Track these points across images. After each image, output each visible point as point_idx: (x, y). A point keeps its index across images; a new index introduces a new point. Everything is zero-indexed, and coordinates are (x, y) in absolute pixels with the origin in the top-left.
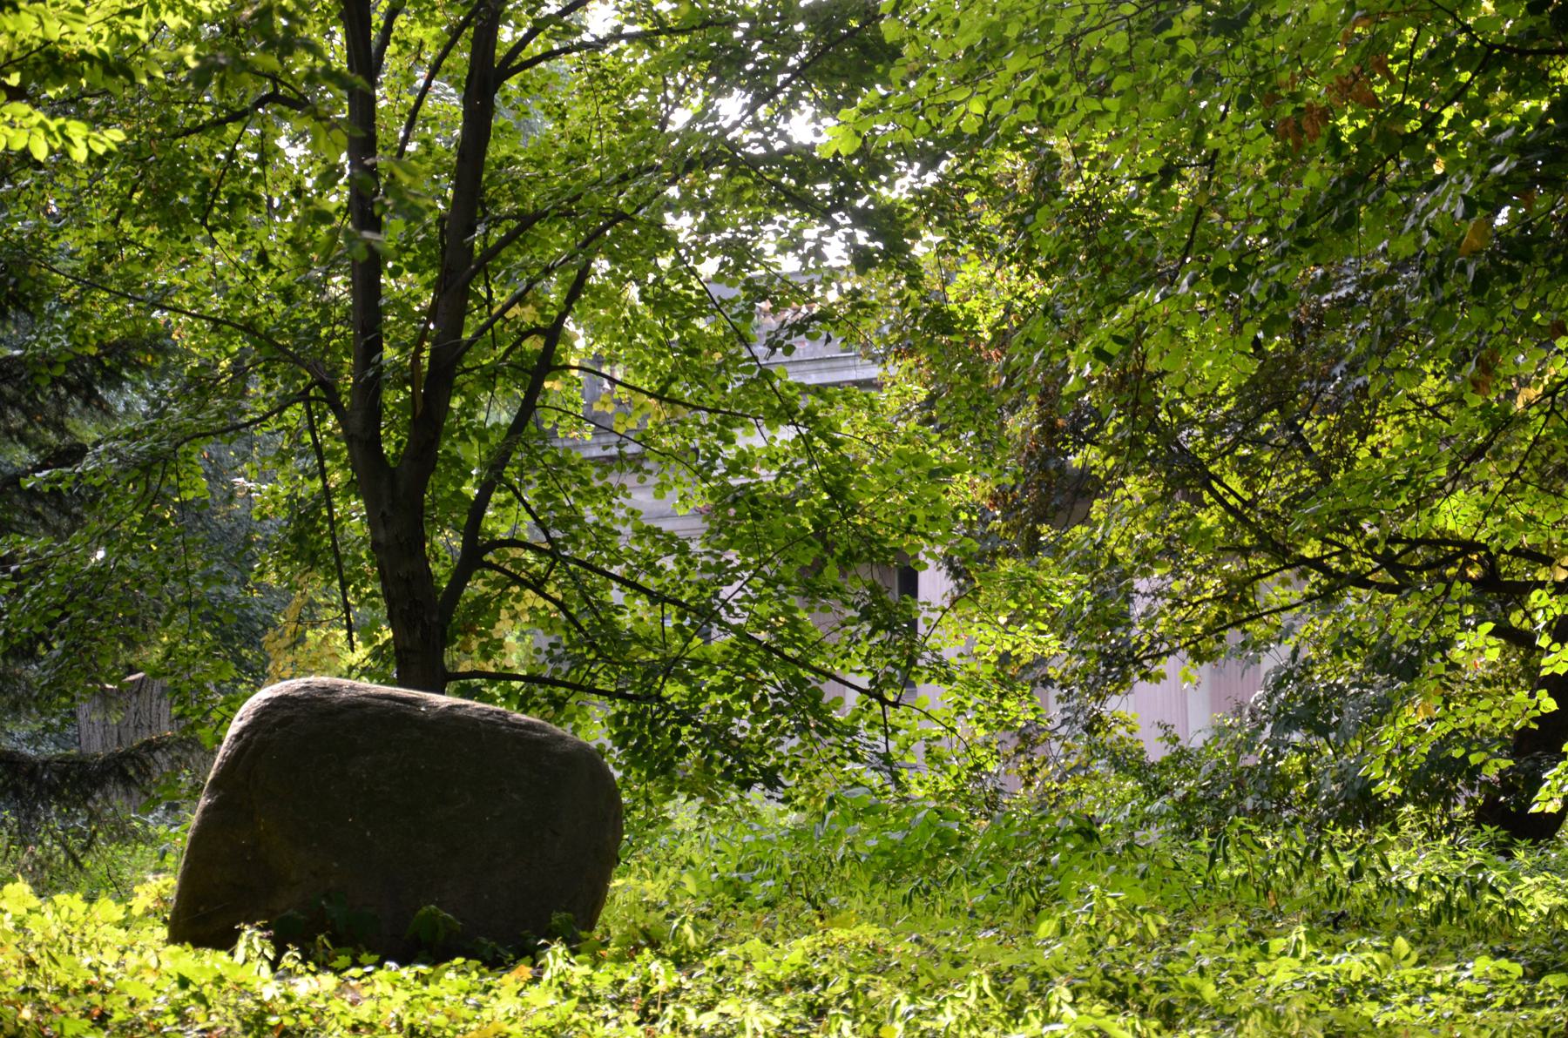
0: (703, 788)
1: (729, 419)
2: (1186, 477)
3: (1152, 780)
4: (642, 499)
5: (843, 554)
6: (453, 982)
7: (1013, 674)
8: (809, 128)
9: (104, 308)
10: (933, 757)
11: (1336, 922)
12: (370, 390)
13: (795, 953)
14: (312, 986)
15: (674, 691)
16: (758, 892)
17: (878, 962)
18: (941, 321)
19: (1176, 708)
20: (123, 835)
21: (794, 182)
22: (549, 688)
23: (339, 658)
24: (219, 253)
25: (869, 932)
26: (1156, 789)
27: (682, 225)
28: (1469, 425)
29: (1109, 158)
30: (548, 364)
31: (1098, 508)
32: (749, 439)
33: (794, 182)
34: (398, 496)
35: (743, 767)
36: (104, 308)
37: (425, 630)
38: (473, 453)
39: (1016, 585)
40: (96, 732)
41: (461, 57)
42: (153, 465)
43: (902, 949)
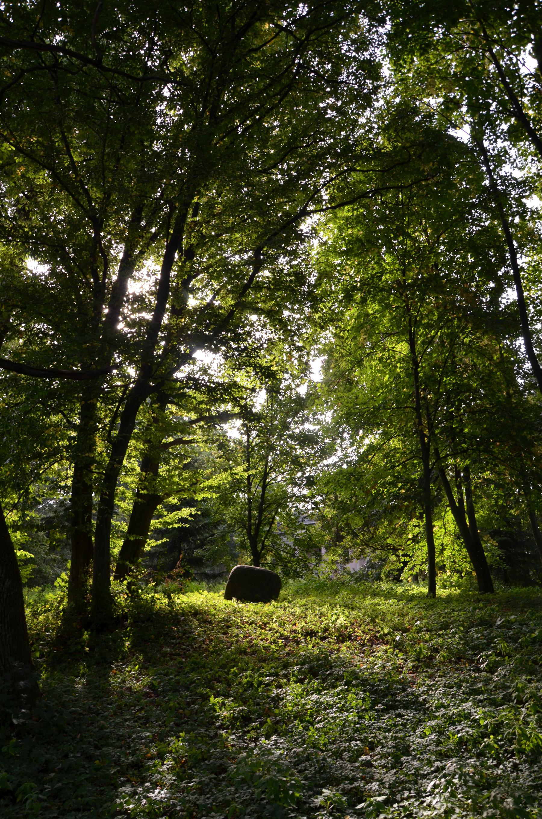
0: (294, 578)
1: (296, 530)
2: (355, 536)
3: (352, 575)
4: (285, 539)
5: (311, 547)
6: (260, 605)
7: (334, 562)
8: (306, 492)
9: (218, 516)
10: (323, 574)
11: (375, 595)
12: (250, 526)
13: (304, 601)
14: (242, 605)
15: (289, 565)
16: (300, 592)
17: (315, 602)
18: (323, 516)
19: (355, 566)
20: (220, 583)
21: (303, 499)
22: (274, 565)
23: (246, 561)
24: (231, 509)
25: (313, 598)
26: (352, 577)
27: (290, 505)
28: (390, 529)
29: (343, 496)
30: (273, 522)
31: (344, 540)
32: (299, 532)
33: (303, 499)
34: (254, 539)
35: (297, 575)
36: (218, 516)
37: (257, 558)
38: (264, 535)
39: (333, 550)
40: (217, 570)
41: (262, 484)
42: (223, 537)
43: (318, 600)
